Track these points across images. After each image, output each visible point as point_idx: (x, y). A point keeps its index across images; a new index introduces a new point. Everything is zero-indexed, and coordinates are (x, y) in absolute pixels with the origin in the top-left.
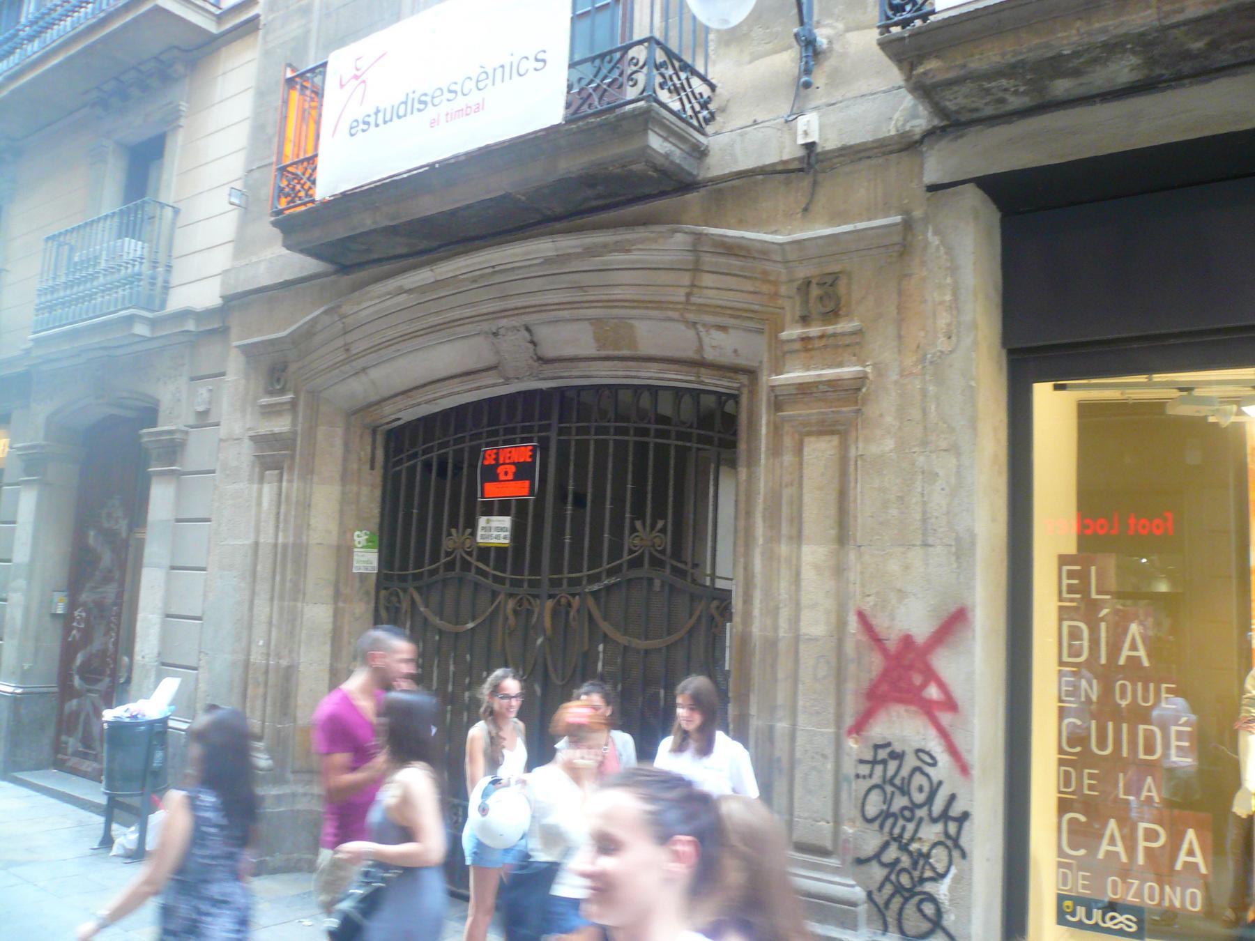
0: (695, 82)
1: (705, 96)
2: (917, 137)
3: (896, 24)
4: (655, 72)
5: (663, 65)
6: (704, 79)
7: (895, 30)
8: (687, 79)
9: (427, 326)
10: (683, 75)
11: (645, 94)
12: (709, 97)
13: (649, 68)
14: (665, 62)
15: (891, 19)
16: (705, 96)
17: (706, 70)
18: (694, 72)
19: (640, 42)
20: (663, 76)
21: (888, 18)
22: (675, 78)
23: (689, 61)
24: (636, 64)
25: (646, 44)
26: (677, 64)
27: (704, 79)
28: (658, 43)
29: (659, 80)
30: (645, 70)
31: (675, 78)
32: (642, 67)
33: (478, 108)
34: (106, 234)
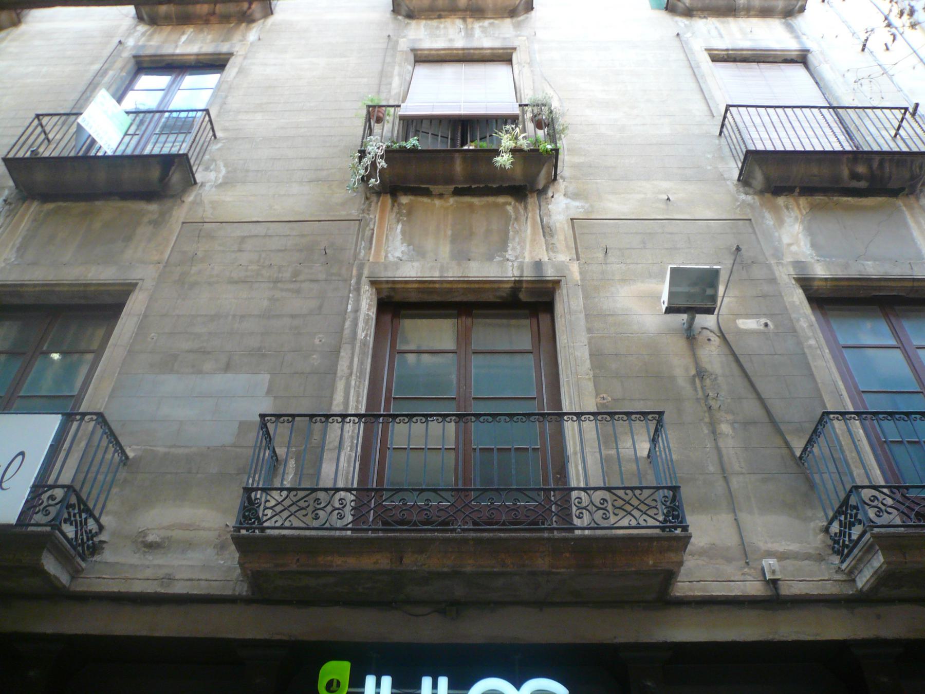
0: (91, 522)
1: (94, 531)
2: (5, 355)
3: (244, 528)
4: (65, 511)
5: (73, 506)
6: (97, 521)
7: (243, 532)
8: (86, 519)
9: (852, 128)
10: (84, 516)
11: (53, 523)
12: (96, 533)
13: (61, 507)
14: (74, 504)
15: (243, 524)
16: (94, 531)
17: (883, 112)
18: (92, 515)
19: (63, 487)
20: (69, 514)
21: (241, 523)
22: (77, 515)
23: (91, 506)
24: (604, 514)
25: (66, 489)
26: (82, 507)
27: (97, 521)
28: (75, 491)
29: (66, 516)
30: (58, 506)
31: (77, 515)
32: (57, 504)
33: (881, 516)
34: (830, 486)
